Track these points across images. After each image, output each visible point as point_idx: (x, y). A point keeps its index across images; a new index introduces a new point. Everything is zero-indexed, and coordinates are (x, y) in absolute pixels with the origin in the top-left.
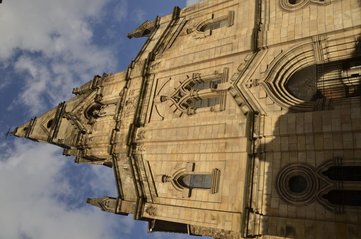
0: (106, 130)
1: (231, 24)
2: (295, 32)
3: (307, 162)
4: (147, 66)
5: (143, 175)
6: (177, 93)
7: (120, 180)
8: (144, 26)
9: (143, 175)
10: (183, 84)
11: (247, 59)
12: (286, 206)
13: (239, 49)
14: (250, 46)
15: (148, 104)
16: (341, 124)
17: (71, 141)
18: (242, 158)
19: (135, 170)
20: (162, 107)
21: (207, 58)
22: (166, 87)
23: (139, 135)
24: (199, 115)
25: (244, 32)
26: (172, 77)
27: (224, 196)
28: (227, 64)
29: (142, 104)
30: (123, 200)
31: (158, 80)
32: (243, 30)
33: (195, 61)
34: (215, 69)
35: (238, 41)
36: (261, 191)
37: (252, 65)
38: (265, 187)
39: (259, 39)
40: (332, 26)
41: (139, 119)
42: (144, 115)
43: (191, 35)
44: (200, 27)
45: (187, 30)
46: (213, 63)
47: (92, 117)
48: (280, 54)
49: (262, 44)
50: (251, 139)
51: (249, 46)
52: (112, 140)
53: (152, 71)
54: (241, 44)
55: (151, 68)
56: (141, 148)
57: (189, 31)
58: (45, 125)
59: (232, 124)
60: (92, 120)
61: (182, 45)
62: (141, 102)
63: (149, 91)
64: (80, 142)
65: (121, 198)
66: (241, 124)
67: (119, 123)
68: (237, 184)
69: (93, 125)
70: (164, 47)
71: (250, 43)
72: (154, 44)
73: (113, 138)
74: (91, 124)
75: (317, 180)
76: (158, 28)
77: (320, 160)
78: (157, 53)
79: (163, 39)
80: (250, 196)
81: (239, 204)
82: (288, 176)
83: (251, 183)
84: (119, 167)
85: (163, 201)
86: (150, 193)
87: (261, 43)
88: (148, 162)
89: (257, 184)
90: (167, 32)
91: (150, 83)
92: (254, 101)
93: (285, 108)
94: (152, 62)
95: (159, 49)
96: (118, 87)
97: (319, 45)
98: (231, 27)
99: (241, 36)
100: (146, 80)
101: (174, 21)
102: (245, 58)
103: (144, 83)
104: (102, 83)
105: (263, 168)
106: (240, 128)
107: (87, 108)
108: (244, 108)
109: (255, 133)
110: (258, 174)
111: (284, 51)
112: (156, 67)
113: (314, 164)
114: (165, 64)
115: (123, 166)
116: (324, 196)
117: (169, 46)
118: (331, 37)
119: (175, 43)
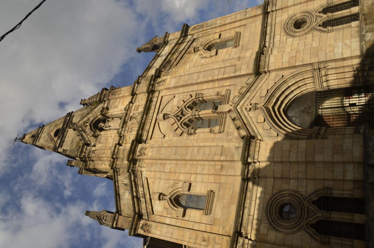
0: (109, 143)
1: (237, 46)
4: (152, 82)
5: (141, 191)
6: (180, 111)
7: (119, 195)
8: (153, 41)
9: (141, 191)
10: (186, 103)
12: (274, 232)
15: (151, 120)
16: (333, 154)
17: (75, 153)
18: (236, 182)
19: (134, 186)
20: (164, 125)
21: (210, 79)
22: (169, 105)
24: (199, 136)
25: (248, 54)
26: (176, 96)
29: (145, 120)
30: (120, 215)
32: (248, 52)
33: (199, 81)
34: (217, 90)
37: (253, 88)
38: (256, 212)
39: (261, 62)
40: (332, 54)
41: (141, 135)
43: (198, 54)
44: (207, 46)
46: (216, 84)
47: (97, 130)
50: (246, 164)
51: (251, 69)
52: (114, 154)
53: (157, 88)
54: (244, 67)
55: (157, 85)
58: (52, 134)
61: (188, 63)
62: (144, 119)
63: (153, 107)
64: (83, 154)
67: (122, 138)
68: (229, 207)
69: (97, 138)
70: (171, 64)
71: (253, 66)
73: (115, 153)
74: (96, 137)
76: (167, 45)
78: (163, 70)
79: (170, 56)
80: (240, 221)
81: (230, 229)
83: (242, 207)
85: (158, 219)
86: (147, 210)
88: (147, 179)
89: (248, 208)
90: (175, 49)
91: (155, 100)
92: (252, 125)
94: (158, 79)
97: (318, 72)
98: (236, 49)
100: (150, 96)
101: (182, 39)
102: (247, 81)
105: (256, 193)
106: (236, 152)
107: (93, 121)
109: (249, 158)
111: (285, 76)
112: (161, 83)
114: (170, 81)
115: (123, 182)
116: (312, 226)
119: (182, 61)
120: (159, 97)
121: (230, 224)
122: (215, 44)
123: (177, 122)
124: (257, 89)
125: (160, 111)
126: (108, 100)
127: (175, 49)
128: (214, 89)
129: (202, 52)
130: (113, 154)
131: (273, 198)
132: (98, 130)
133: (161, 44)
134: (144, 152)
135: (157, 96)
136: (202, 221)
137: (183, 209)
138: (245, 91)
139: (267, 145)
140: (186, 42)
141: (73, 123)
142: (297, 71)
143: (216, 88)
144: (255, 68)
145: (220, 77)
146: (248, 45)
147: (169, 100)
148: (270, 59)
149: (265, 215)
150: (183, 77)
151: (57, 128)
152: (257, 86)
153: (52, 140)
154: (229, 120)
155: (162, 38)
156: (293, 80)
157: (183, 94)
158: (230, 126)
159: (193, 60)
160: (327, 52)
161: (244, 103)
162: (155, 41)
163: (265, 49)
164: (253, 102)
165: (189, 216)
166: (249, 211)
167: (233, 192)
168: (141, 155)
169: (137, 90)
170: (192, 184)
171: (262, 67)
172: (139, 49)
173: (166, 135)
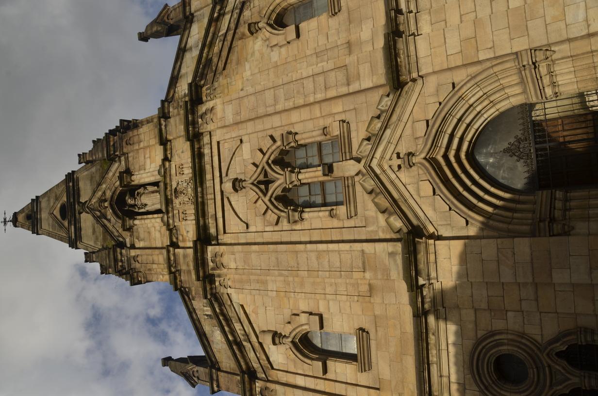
0: (155, 240)
1: (337, 11)
2: (476, 40)
3: (526, 332)
5: (240, 330)
6: (260, 174)
7: (205, 334)
8: (164, 16)
11: (382, 106)
13: (362, 82)
14: (384, 75)
15: (213, 195)
17: (106, 261)
18: (404, 314)
19: (224, 323)
20: (241, 202)
21: (300, 101)
22: (237, 159)
23: (214, 260)
24: (311, 224)
25: (365, 32)
26: (245, 139)
27: (382, 379)
28: (345, 112)
29: (203, 197)
30: (219, 369)
31: (218, 143)
32: (364, 27)
33: (279, 107)
34: (322, 123)
35: (356, 61)
36: (446, 377)
37: (394, 118)
38: (453, 370)
39: (400, 58)
40: (562, 25)
42: (211, 218)
43: (260, 38)
44: (274, 17)
45: (249, 25)
46: (316, 111)
47: (125, 217)
48: (450, 92)
49: (410, 73)
50: (415, 288)
51: (381, 74)
52: (172, 266)
53: (205, 128)
54: (365, 69)
55: (200, 120)
56: (223, 281)
57: (253, 29)
58: (57, 213)
59: (375, 253)
60: (127, 224)
61: (246, 63)
62: (199, 195)
63: (208, 167)
65: (215, 368)
66: (392, 254)
68: (401, 360)
69: (132, 230)
70: (214, 68)
72: (192, 58)
73: (172, 262)
74: (130, 229)
75: (547, 369)
76: (191, 22)
77: (550, 329)
78: (202, 82)
80: (428, 388)
82: (492, 354)
83: (426, 365)
84: (197, 311)
86: (260, 362)
87: (405, 68)
88: (242, 306)
89: (437, 364)
90: (211, 35)
91: (206, 151)
92: (411, 201)
93: (473, 222)
94: (199, 107)
95: (205, 72)
96: (153, 154)
97: (533, 71)
98: (336, 17)
99: (361, 43)
100: (196, 146)
101: (218, 8)
102: (379, 104)
103: (196, 153)
104: (122, 147)
105: (446, 335)
106: (392, 262)
107: (112, 197)
108: (393, 221)
109: (420, 277)
110: (436, 347)
111: (458, 85)
112: (208, 116)
113: (540, 336)
114: (224, 110)
115: (204, 311)
117: (223, 65)
118: (559, 50)
119: (233, 57)
120: (212, 144)
121: (410, 389)
122: (288, 7)
123: (263, 198)
124: (405, 120)
125: (224, 175)
126: (124, 154)
127: (211, 35)
128: (315, 120)
129: (268, 34)
130: (170, 266)
131: (480, 347)
132: (127, 218)
133: (180, 21)
134: (220, 261)
135: (208, 144)
136: (360, 382)
137: (321, 363)
138: (380, 129)
139: (450, 249)
140: (228, 12)
141: (81, 203)
142: (484, 71)
143: (317, 118)
144: (391, 76)
145: (320, 96)
146: (359, 8)
147: (234, 150)
148: (418, 47)
149: (470, 376)
150: (246, 100)
151: (61, 202)
152: (402, 113)
153: (61, 226)
154: (361, 196)
155: (178, 7)
156: (478, 92)
157: (255, 135)
158: (366, 206)
159: (254, 52)
160: (548, 21)
161: (384, 153)
162: (166, 16)
163: (401, 18)
164: (403, 150)
165: (334, 372)
166: (440, 369)
167: (403, 333)
168: (217, 267)
169: (168, 132)
170: (324, 316)
171: (404, 70)
172: (142, 37)
173: (249, 223)
